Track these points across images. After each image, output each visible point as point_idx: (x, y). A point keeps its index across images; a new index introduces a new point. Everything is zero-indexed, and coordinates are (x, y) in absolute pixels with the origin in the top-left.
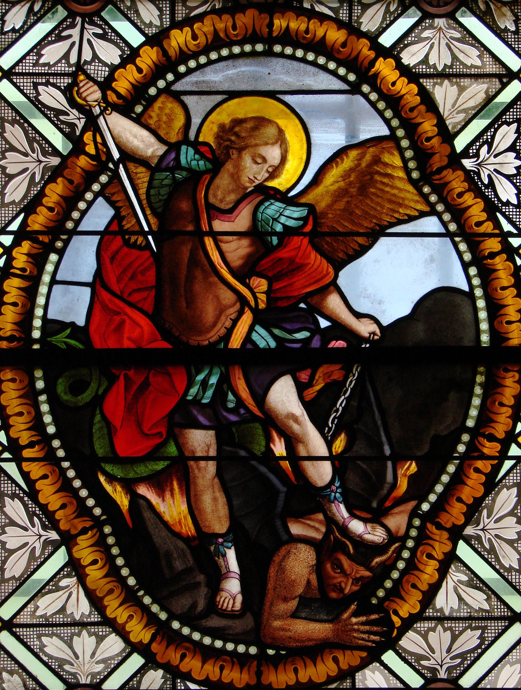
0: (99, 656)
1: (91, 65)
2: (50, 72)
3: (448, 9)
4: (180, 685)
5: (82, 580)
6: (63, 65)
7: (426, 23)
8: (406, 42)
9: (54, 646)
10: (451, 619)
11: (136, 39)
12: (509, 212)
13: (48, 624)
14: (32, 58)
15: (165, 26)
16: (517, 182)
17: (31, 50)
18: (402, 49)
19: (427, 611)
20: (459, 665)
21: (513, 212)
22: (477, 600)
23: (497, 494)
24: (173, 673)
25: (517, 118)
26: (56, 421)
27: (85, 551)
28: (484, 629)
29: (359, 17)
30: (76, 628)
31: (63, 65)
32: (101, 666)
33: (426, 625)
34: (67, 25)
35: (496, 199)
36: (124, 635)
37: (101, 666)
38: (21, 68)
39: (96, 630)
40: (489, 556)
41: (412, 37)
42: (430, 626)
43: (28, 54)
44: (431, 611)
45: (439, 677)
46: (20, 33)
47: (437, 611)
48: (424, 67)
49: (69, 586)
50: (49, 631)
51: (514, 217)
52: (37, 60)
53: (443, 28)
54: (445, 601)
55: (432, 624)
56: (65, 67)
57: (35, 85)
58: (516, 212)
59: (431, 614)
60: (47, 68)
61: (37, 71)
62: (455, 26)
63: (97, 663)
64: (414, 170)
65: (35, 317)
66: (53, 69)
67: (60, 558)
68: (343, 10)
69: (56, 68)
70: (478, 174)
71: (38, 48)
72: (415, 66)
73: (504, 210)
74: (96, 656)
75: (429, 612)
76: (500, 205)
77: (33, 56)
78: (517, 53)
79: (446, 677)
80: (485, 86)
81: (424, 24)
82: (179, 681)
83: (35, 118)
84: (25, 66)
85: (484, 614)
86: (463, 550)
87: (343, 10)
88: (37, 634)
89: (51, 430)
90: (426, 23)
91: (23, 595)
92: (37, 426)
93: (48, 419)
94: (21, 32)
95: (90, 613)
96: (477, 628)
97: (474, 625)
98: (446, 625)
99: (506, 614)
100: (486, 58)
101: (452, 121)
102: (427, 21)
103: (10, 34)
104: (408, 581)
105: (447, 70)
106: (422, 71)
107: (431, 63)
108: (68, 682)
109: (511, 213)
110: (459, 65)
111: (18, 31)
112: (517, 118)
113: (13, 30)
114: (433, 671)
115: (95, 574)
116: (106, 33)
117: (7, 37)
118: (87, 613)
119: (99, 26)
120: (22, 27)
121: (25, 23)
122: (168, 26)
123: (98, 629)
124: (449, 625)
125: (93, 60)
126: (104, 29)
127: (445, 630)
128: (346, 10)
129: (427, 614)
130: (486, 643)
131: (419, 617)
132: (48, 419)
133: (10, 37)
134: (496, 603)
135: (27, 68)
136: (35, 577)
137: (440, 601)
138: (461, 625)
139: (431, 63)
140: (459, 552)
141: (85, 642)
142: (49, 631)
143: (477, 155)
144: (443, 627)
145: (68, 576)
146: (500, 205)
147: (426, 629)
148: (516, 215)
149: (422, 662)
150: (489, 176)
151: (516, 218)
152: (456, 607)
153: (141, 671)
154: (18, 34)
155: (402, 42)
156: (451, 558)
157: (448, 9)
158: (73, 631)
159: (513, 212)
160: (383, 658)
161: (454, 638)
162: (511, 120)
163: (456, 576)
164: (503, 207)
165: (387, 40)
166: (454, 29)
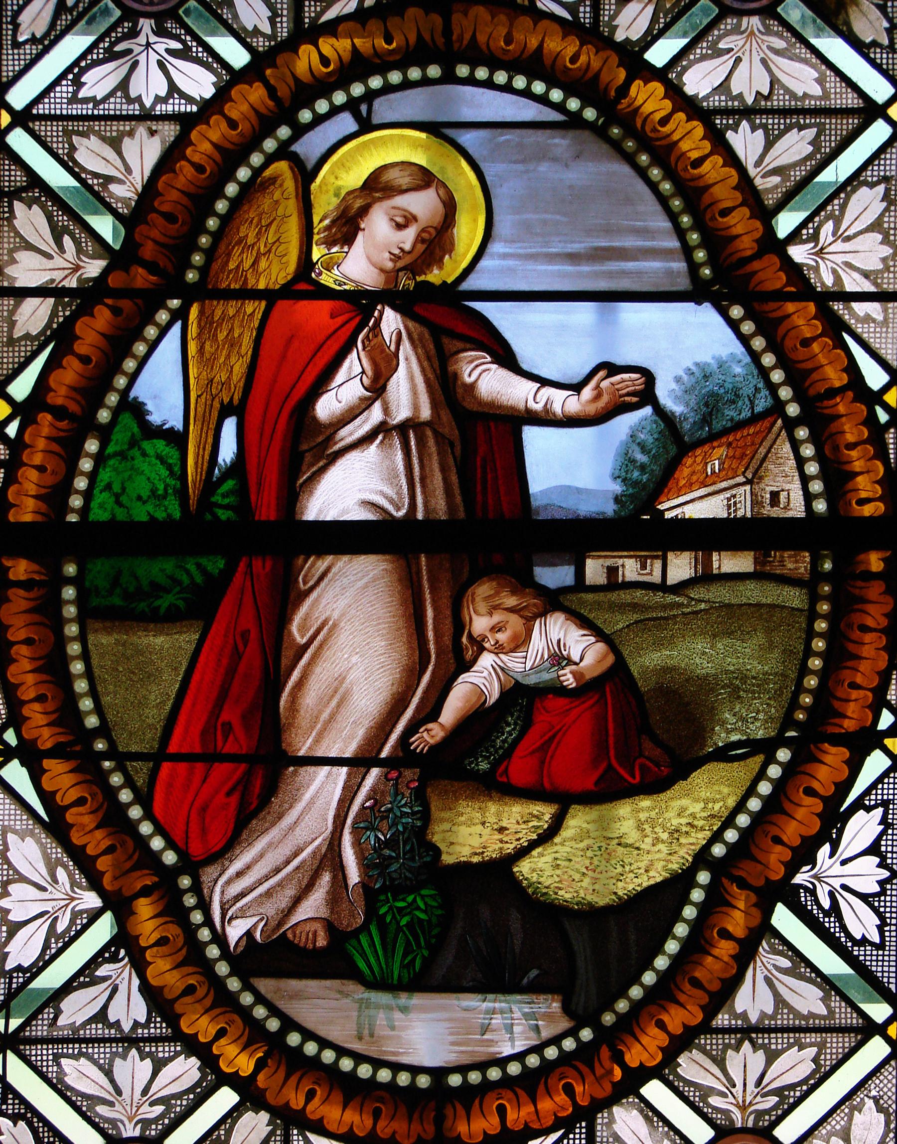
1: (166, 103)
2: (96, 112)
4: (585, 13)
5: (139, 965)
6: (118, 100)
7: (156, 1129)
8: (191, 1096)
9: (81, 1074)
10: (759, 1029)
11: (236, 55)
14: (65, 90)
15: (606, 1115)
17: (63, 76)
18: (198, 1084)
19: (720, 1016)
20: (119, 40)
23: (48, 326)
24: (288, 1119)
28: (74, 99)
29: (613, 18)
31: (118, 100)
33: (170, 108)
34: (123, 32)
38: (47, 106)
39: (153, 1049)
40: (825, 924)
41: (702, 48)
42: (164, 106)
43: (57, 82)
44: (726, 1016)
45: (153, 21)
46: (46, 43)
47: (737, 1016)
48: (723, 98)
50: (73, 1049)
52: (76, 93)
53: (126, 1122)
54: (751, 1000)
55: (159, 109)
56: (121, 103)
57: (68, 134)
59: (726, 1022)
60: (91, 106)
61: (74, 112)
62: (106, 1126)
63: (730, 50)
66: (101, 107)
69: (106, 106)
71: (75, 72)
72: (177, 1054)
75: (722, 1020)
77: (67, 85)
78: (885, 73)
79: (142, 21)
81: (160, 1127)
82: (295, 1132)
83: (67, 188)
84: (55, 103)
85: (817, 1022)
86: (783, 918)
88: (53, 1054)
90: (156, 1129)
94: (46, 42)
96: (86, 100)
97: (91, 106)
98: (137, 107)
99: (854, 1021)
102: (153, 1133)
103: (28, 47)
105: (120, 1050)
106: (164, 1046)
107: (148, 1062)
110: (784, 95)
111: (40, 41)
113: (33, 40)
114: (161, 32)
116: (187, 48)
117: (22, 51)
119: (177, 38)
120: (47, 34)
121: (52, 25)
122: (600, 1115)
123: (157, 1047)
124: (131, 107)
125: (170, 95)
126: (183, 42)
127: (139, 99)
130: (70, 77)
133: (28, 51)
134: (837, 1004)
135: (58, 106)
138: (111, 107)
139: (148, 1062)
140: (775, 921)
141: (134, 1070)
142: (73, 1049)
144: (142, 105)
145: (114, 959)
147: (171, 101)
149: (179, 46)
152: (770, 1010)
153: (232, 1116)
154: (40, 47)
155: (200, 1095)
158: (114, 1050)
160: (644, 1091)
161: (124, 85)
163: (768, 958)
165: (225, 1098)
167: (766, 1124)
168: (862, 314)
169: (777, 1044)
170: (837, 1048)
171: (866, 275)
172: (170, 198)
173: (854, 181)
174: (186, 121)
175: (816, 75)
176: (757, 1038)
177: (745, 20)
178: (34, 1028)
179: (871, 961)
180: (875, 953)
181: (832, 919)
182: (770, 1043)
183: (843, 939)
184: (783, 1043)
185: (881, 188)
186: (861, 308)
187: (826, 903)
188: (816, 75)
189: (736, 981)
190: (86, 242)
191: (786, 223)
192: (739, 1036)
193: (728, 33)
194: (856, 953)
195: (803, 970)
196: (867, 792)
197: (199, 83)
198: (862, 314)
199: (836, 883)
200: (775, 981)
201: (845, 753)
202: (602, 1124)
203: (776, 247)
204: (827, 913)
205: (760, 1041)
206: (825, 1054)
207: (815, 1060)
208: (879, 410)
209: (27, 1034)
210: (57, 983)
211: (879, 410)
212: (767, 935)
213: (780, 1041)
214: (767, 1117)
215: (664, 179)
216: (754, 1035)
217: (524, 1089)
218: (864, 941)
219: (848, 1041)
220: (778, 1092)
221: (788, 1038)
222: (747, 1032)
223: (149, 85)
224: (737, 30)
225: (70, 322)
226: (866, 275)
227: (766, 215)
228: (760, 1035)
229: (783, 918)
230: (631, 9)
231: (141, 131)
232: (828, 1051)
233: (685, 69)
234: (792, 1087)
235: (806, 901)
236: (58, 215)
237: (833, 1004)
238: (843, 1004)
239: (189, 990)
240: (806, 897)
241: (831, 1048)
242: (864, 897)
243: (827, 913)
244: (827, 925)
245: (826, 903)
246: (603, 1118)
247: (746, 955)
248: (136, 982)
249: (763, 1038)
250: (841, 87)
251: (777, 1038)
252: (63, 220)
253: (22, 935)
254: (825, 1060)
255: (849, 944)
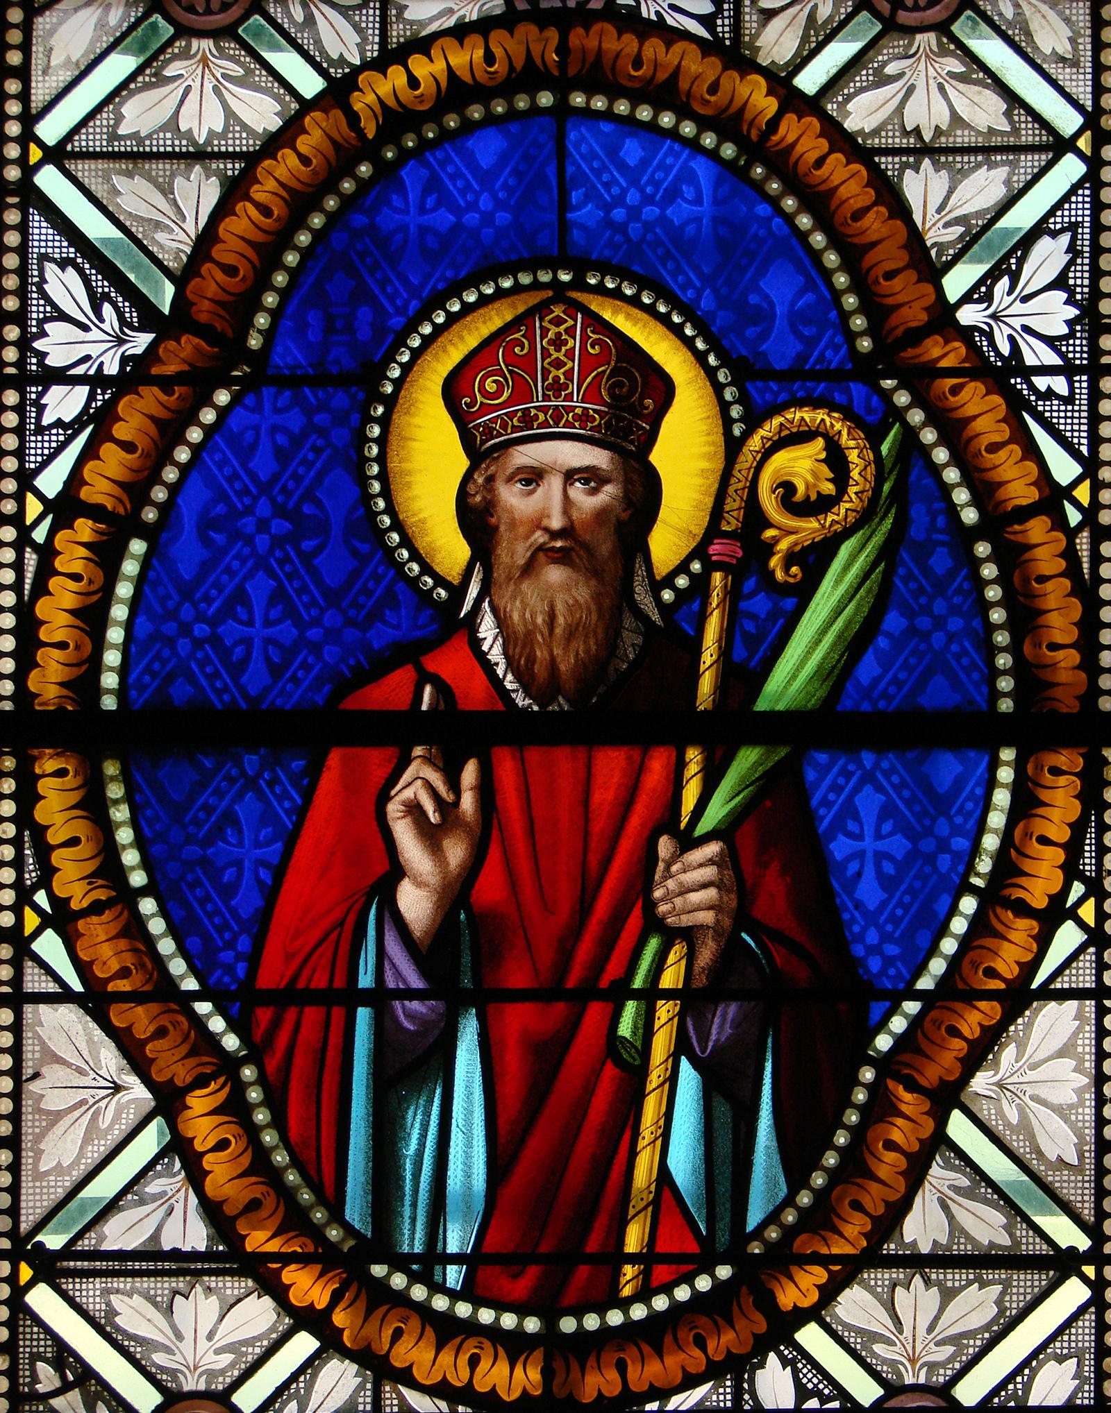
0: (222, 1339)
3: (935, 14)
5: (196, 1177)
8: (846, 91)
12: (1051, 411)
13: (988, 150)
15: (369, 54)
16: (1068, 352)
21: (1059, 411)
22: (986, 1226)
25: (1070, 222)
26: (147, 864)
27: (202, 1124)
30: (181, 1279)
32: (227, 1358)
35: (1025, 386)
36: (835, 133)
37: (227, 1358)
49: (165, 1193)
51: (1062, 421)
54: (922, 1227)
58: (1066, 411)
62: (165, 1377)
64: (252, 1084)
65: (106, 645)
67: (150, 1141)
68: (723, 18)
70: (990, 336)
73: (1040, 408)
74: (216, 1338)
76: (1033, 398)
80: (1002, 172)
86: (959, 1128)
87: (723, 18)
89: (138, 879)
91: (1007, 232)
92: (108, 867)
93: (130, 857)
95: (901, 177)
99: (80, 167)
100: (100, 1311)
101: (172, 1182)
104: (405, 1320)
108: (166, 1387)
109: (1055, 414)
112: (1070, 222)
115: (221, 1173)
118: (909, 173)
128: (729, 17)
129: (237, 166)
131: (252, 160)
132: (130, 857)
134: (1024, 1233)
136: (87, 1193)
137: (211, 194)
143: (988, 298)
145: (941, 247)
146: (1033, 398)
148: (1066, 417)
150: (1011, 339)
151: (1066, 424)
156: (940, 1141)
157: (935, 14)
159: (1059, 411)
162: (1058, 226)
163: (939, 1175)
164: (1040, 403)
165: (809, 80)
166: (163, 1369)
167: (177, 44)
168: (1043, 389)
169: (165, 139)
170: (1025, 1287)
171: (1050, 341)
172: (229, 249)
173: (1039, 230)
174: (872, 1258)
175: (117, 1319)
176: (187, 146)
177: (202, 1386)
178: (1036, 164)
179: (54, 241)
180: (50, 250)
181: (100, 290)
182: (172, 139)
183: (87, 266)
184: (158, 140)
185: (1065, 239)
186: (1041, 383)
187: (107, 309)
188: (117, 1319)
189: (905, 1205)
190: (990, 1114)
191: (956, 282)
192: (209, 149)
193: (222, 1372)
194: (72, 250)
195: (983, 1190)
196: (62, 447)
197: (261, 113)
198: (1043, 389)
199: (95, 334)
200: (949, 1202)
201: (85, 494)
202: (373, 43)
203: (943, 313)
204: (106, 297)
205: (184, 142)
206: (108, 126)
207: (999, 1302)
208: (1069, 508)
209: (1044, 157)
210: (111, 1193)
211: (1069, 508)
212: (943, 1147)
213: (161, 142)
214: (176, 51)
215: (296, 1189)
216: (191, 149)
217: (649, 1343)
218: (63, 264)
219: (81, 142)
220: (955, 1340)
221: (151, 146)
222: (916, 1262)
223: (202, 120)
224: (211, 1374)
225: (110, 405)
226: (1050, 341)
227: (934, 272)
228: (184, 149)
229: (165, 295)
230: (339, 1399)
231: (925, 1249)
232: (105, 130)
233: (273, 1329)
234: (147, 87)
235: (131, 312)
236: (97, 281)
237: (1018, 1233)
238: (1031, 1233)
239: (253, 1205)
240: (131, 317)
241: (101, 133)
242: (63, 317)
243: (106, 297)
244: (106, 283)
245: (107, 309)
246: (372, 51)
247: (916, 1176)
248: (193, 1200)
249: (180, 146)
250: (87, 1304)
251: (165, 146)
252: (103, 287)
253: (1050, 274)
254: (1011, 1301)
255: (79, 260)
